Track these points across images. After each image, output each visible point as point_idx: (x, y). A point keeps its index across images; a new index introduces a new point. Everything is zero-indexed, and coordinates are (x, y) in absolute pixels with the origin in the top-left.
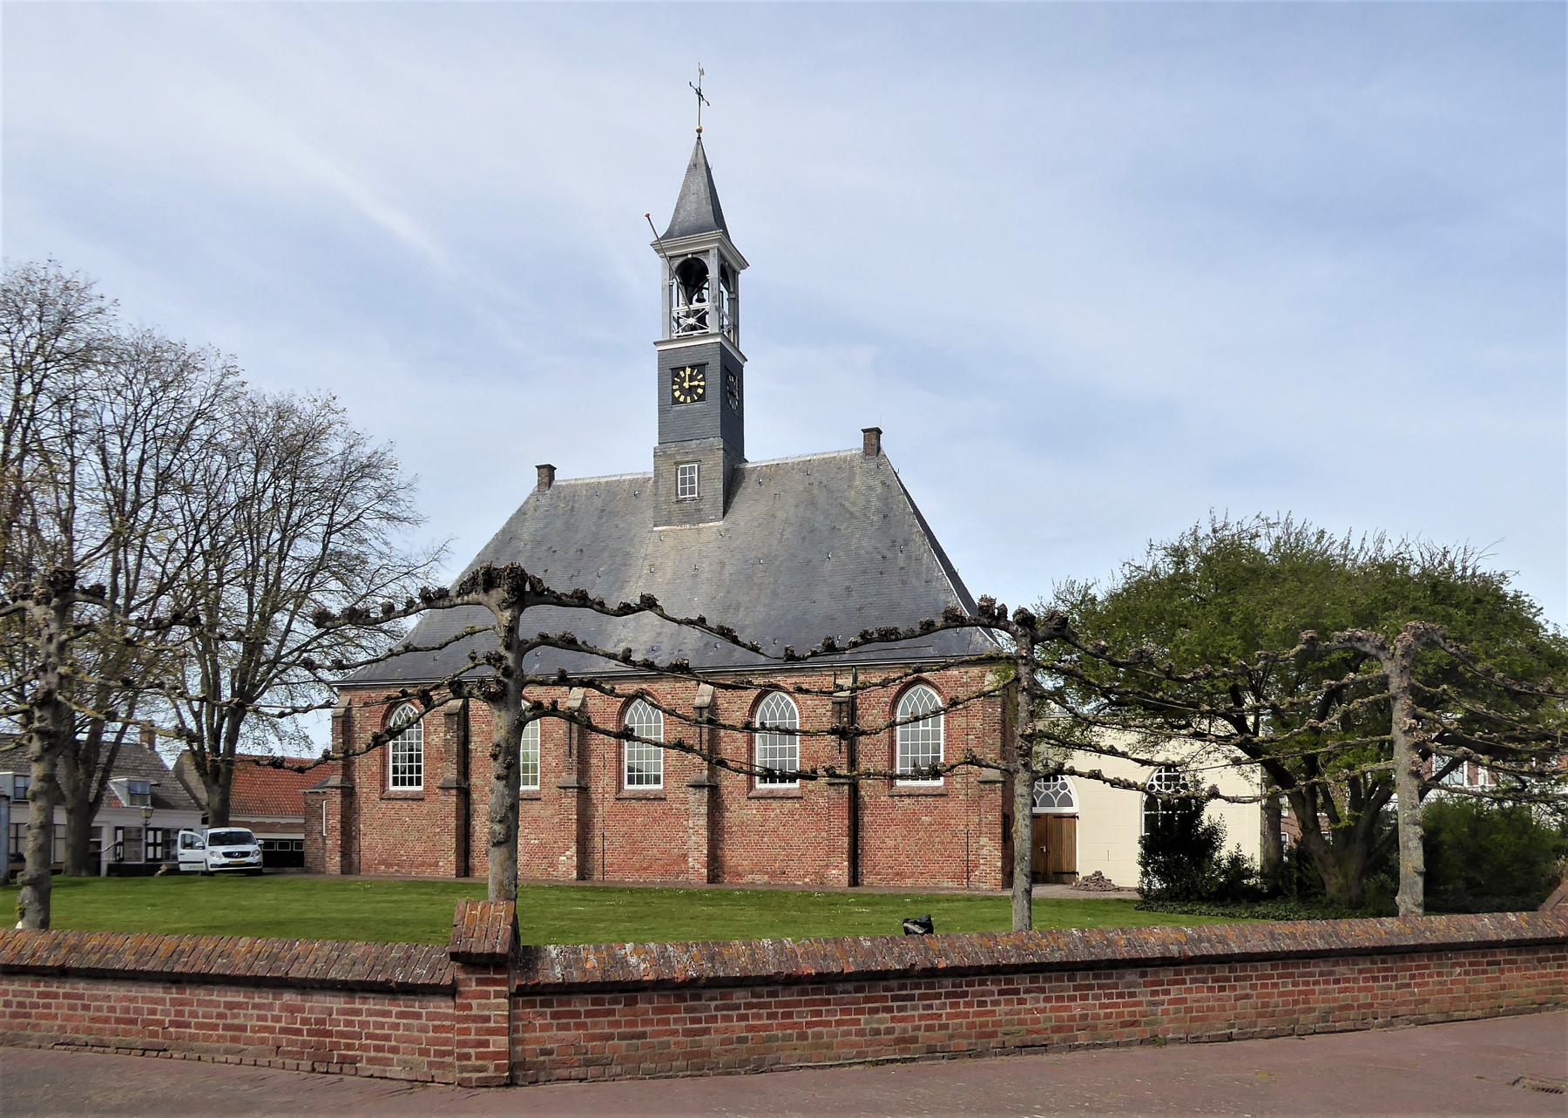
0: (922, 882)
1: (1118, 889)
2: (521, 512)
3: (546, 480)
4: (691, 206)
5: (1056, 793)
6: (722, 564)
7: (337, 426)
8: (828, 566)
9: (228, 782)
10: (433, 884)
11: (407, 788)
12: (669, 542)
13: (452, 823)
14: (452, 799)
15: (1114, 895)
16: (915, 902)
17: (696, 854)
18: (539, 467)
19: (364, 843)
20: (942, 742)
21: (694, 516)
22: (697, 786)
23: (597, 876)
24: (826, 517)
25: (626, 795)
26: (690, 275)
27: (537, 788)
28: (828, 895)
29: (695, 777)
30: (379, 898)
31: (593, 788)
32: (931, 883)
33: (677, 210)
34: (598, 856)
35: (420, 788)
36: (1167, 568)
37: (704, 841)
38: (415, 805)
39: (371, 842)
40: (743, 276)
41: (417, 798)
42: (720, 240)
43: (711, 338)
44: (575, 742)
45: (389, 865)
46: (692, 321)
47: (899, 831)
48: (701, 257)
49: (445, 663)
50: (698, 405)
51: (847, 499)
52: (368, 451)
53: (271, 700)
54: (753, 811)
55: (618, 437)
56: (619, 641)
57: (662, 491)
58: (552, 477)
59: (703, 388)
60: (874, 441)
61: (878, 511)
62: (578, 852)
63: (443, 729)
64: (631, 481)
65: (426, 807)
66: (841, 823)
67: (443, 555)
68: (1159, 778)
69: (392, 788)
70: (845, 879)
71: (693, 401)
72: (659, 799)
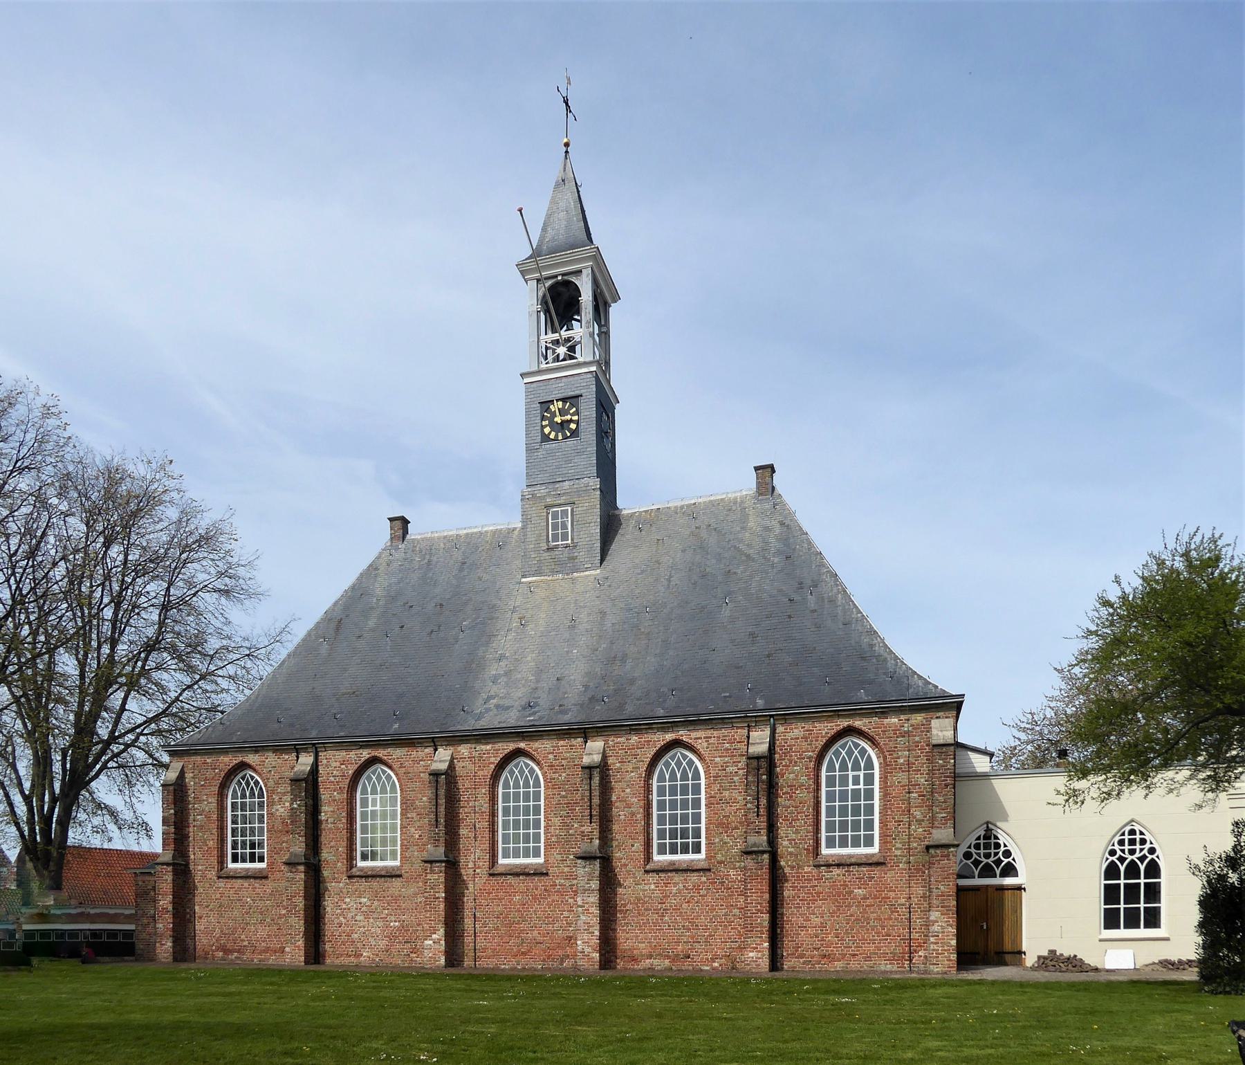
0: (854, 965)
2: (373, 568)
4: (561, 219)
5: (998, 862)
6: (603, 614)
8: (726, 612)
9: (60, 866)
10: (279, 971)
13: (300, 902)
15: (1091, 976)
18: (391, 520)
19: (200, 926)
20: (877, 802)
21: (569, 565)
22: (587, 858)
23: (468, 962)
25: (498, 870)
26: (560, 303)
27: (397, 863)
29: (584, 847)
30: (212, 989)
31: (462, 861)
32: (866, 966)
34: (468, 940)
35: (263, 865)
38: (257, 883)
40: (614, 310)
41: (260, 876)
44: (442, 809)
47: (824, 906)
48: (573, 279)
49: (292, 725)
51: (741, 541)
54: (651, 884)
55: (481, 490)
56: (490, 698)
57: (531, 537)
58: (405, 532)
59: (577, 422)
62: (447, 935)
63: (288, 797)
64: (494, 532)
65: (269, 886)
66: (759, 896)
68: (1121, 843)
69: (231, 865)
70: (765, 963)
71: (565, 438)
72: (540, 873)
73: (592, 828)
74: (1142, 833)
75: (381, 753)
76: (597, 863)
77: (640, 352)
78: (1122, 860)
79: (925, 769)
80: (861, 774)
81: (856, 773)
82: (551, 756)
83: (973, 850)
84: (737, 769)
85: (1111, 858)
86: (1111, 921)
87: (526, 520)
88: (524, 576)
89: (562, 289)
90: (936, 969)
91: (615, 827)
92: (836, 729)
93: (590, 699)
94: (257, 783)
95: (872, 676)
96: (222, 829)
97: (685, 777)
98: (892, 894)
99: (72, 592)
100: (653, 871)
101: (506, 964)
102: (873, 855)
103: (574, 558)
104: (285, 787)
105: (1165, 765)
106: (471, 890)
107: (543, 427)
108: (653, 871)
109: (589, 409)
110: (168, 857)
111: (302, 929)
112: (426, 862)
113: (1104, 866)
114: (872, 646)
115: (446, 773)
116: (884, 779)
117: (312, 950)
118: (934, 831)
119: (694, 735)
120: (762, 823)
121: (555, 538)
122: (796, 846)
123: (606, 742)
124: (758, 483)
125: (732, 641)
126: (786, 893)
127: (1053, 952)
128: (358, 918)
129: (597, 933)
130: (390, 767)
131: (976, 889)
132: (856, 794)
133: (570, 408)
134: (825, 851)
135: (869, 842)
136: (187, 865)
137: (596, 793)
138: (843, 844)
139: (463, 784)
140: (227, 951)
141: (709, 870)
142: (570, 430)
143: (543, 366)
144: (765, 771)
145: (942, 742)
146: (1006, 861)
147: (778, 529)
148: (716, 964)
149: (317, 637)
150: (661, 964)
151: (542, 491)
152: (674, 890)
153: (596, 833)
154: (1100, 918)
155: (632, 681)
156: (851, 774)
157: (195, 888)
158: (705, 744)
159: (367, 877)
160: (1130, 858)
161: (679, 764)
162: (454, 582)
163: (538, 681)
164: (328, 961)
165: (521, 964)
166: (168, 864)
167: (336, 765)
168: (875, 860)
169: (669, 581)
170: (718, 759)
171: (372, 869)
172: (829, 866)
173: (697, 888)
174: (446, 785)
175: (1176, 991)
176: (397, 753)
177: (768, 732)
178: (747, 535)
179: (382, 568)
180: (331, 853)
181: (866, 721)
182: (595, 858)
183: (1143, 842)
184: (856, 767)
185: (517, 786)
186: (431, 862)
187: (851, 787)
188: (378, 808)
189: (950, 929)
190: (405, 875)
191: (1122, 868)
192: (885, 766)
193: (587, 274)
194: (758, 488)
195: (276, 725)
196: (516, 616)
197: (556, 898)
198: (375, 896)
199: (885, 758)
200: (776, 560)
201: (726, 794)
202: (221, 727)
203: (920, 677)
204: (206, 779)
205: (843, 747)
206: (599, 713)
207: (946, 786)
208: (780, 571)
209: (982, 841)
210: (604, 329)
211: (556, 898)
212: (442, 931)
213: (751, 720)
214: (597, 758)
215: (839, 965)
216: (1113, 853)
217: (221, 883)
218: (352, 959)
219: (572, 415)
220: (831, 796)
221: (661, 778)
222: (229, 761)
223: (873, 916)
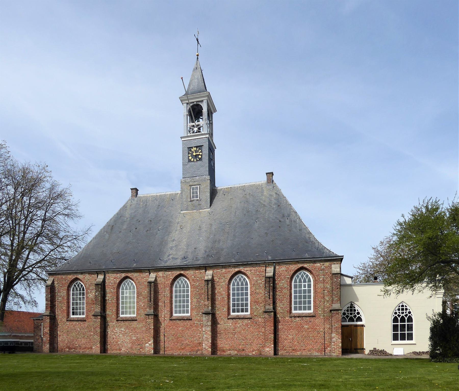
0: (304, 353)
2: (125, 207)
3: (135, 194)
5: (355, 316)
6: (211, 225)
7: (48, 178)
8: (256, 225)
13: (99, 330)
14: (99, 320)
17: (206, 342)
18: (131, 189)
19: (59, 339)
21: (198, 207)
23: (162, 352)
26: (195, 112)
27: (135, 315)
29: (205, 310)
32: (308, 353)
34: (162, 344)
36: (412, 218)
37: (210, 337)
38: (82, 323)
39: (63, 339)
40: (214, 115)
41: (83, 320)
43: (202, 139)
44: (152, 295)
45: (70, 349)
47: (294, 332)
48: (200, 104)
50: (199, 162)
52: (60, 189)
53: (19, 288)
57: (184, 196)
58: (137, 194)
59: (201, 155)
61: (275, 204)
63: (94, 291)
64: (170, 195)
65: (86, 324)
67: (89, 232)
68: (399, 310)
70: (272, 352)
72: (189, 319)
73: (208, 303)
74: (406, 306)
75: (129, 275)
80: (307, 284)
81: (305, 284)
82: (193, 276)
83: (346, 312)
84: (262, 281)
85: (395, 315)
86: (395, 338)
87: (182, 190)
88: (181, 211)
90: (334, 354)
91: (217, 303)
94: (82, 285)
95: (310, 249)
96: (68, 302)
98: (318, 327)
100: (231, 319)
101: (176, 353)
102: (311, 313)
103: (200, 205)
107: (189, 157)
108: (231, 319)
109: (206, 150)
111: (99, 340)
114: (310, 238)
116: (315, 286)
117: (103, 348)
119: (246, 269)
120: (271, 301)
121: (193, 197)
122: (283, 310)
123: (213, 271)
124: (267, 179)
126: (279, 327)
127: (375, 349)
128: (120, 336)
130: (133, 280)
132: (305, 291)
134: (293, 312)
135: (309, 308)
136: (55, 316)
137: (210, 290)
138: (300, 309)
139: (160, 287)
140: (70, 349)
141: (251, 318)
142: (199, 158)
143: (189, 135)
144: (272, 282)
145: (336, 273)
146: (358, 316)
148: (254, 353)
149: (105, 232)
150: (233, 353)
151: (188, 180)
152: (239, 325)
153: (210, 304)
154: (391, 337)
155: (222, 250)
156: (303, 284)
157: (58, 325)
158: (250, 273)
159: (124, 320)
160: (402, 315)
162: (155, 212)
163: (187, 249)
164: (109, 352)
166: (48, 316)
167: (112, 279)
168: (312, 315)
169: (235, 213)
170: (254, 278)
171: (126, 317)
172: (295, 317)
173: (247, 325)
174: (154, 287)
176: (135, 275)
177: (273, 268)
179: (128, 207)
180: (110, 312)
181: (308, 265)
182: (209, 314)
183: (406, 309)
184: (305, 281)
185: (180, 287)
186: (148, 315)
187: (303, 288)
188: (128, 295)
190: (138, 320)
191: (399, 319)
192: (315, 281)
193: (205, 102)
194: (267, 181)
199: (315, 278)
200: (274, 206)
201: (258, 290)
205: (300, 274)
206: (211, 261)
207: (337, 288)
208: (276, 211)
209: (349, 309)
212: (152, 341)
213: (266, 264)
214: (210, 277)
215: (299, 353)
216: (396, 313)
217: (68, 323)
219: (200, 152)
220: (296, 292)
221: (234, 285)
222: (71, 277)
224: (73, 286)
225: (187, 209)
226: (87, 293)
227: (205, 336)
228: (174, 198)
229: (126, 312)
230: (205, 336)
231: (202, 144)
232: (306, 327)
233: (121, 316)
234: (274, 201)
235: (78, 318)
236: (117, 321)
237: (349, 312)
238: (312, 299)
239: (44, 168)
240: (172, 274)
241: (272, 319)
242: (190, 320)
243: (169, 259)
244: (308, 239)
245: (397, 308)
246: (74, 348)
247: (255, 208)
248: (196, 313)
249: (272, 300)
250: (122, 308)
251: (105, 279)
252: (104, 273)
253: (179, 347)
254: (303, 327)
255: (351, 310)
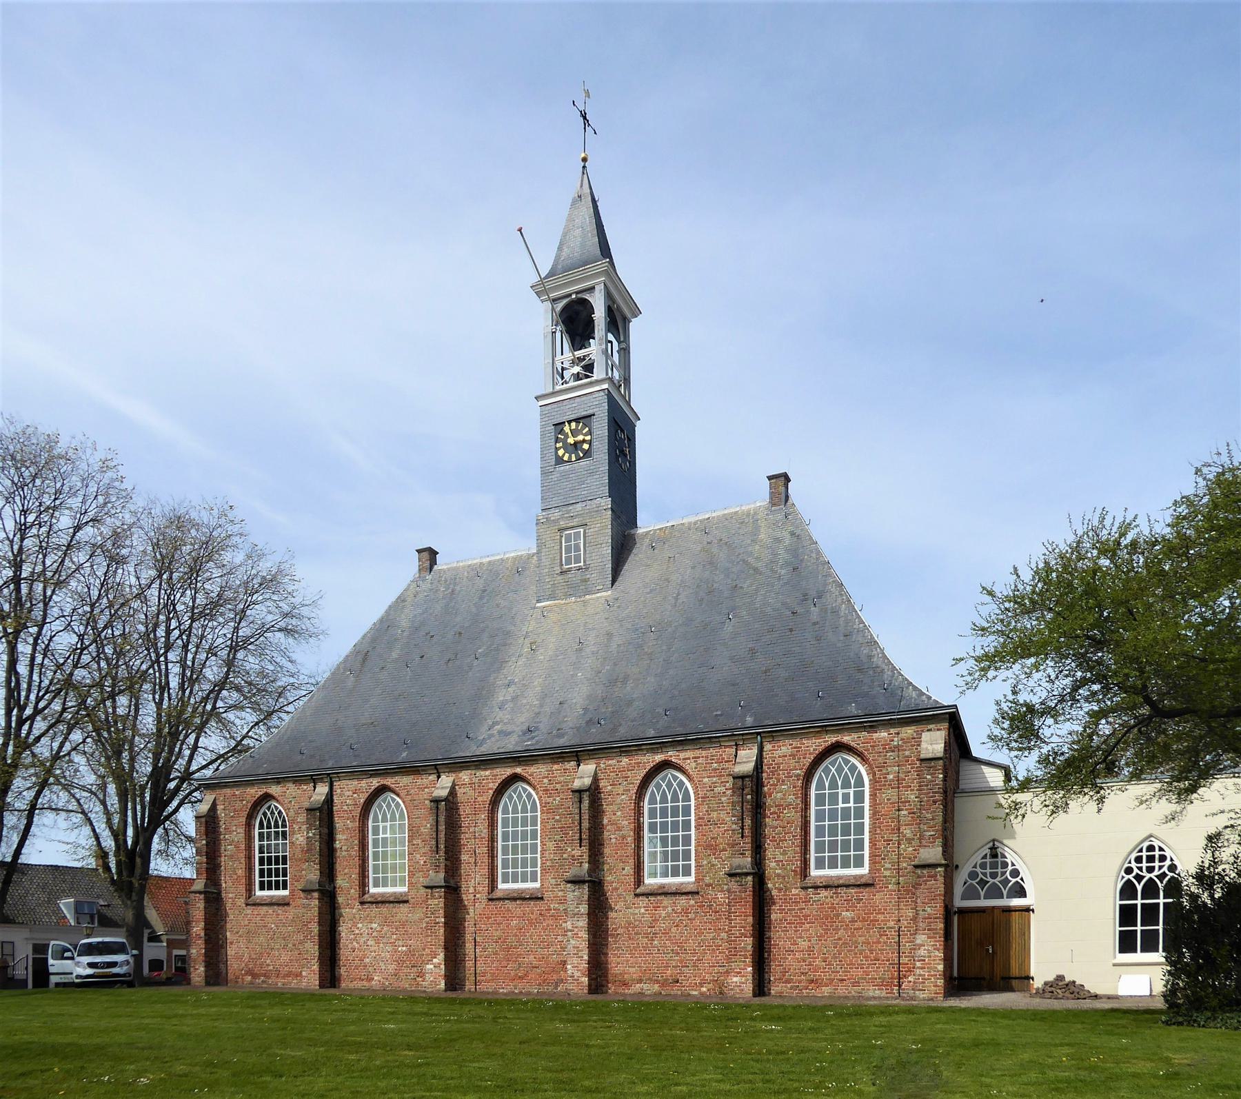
0: (842, 990)
1: (1096, 996)
2: (401, 600)
3: (427, 564)
5: (1007, 881)
7: (235, 539)
8: (729, 628)
11: (273, 893)
12: (553, 617)
13: (315, 928)
15: (1087, 1004)
16: (839, 1015)
18: (419, 551)
19: (231, 951)
20: (867, 821)
21: (581, 588)
22: (576, 882)
23: (469, 986)
24: (727, 576)
26: (575, 322)
27: (405, 889)
28: (727, 1007)
32: (854, 991)
33: (560, 248)
34: (469, 964)
35: (286, 893)
38: (280, 910)
39: (237, 951)
40: (635, 326)
42: (606, 273)
44: (442, 836)
45: (254, 976)
46: (577, 369)
47: (813, 930)
48: (587, 296)
49: (312, 756)
50: (583, 463)
58: (433, 562)
59: (590, 443)
60: (782, 489)
61: (787, 564)
62: (447, 959)
64: (515, 559)
65: (291, 912)
66: (744, 920)
68: (1139, 860)
69: (259, 893)
71: (579, 459)
72: (536, 898)
73: (582, 852)
74: (1161, 849)
75: (389, 781)
76: (586, 886)
77: (662, 368)
78: (1139, 878)
79: (915, 785)
80: (851, 791)
81: (846, 791)
82: (546, 781)
83: (978, 870)
84: (725, 789)
85: (1127, 877)
86: (1127, 943)
87: (541, 545)
88: (538, 601)
89: (577, 307)
90: (921, 995)
91: (607, 851)
92: (824, 745)
93: (587, 723)
94: (280, 813)
95: (866, 688)
96: (249, 858)
97: (675, 798)
98: (881, 917)
99: (149, 639)
100: (643, 895)
101: (505, 988)
102: (862, 876)
103: (586, 581)
104: (302, 818)
105: (1137, 776)
106: (472, 914)
107: (557, 449)
108: (643, 895)
109: (601, 428)
110: (199, 885)
111: (317, 954)
112: (427, 887)
113: (1120, 886)
114: (870, 657)
115: (446, 799)
116: (873, 796)
117: (328, 975)
118: (922, 850)
119: (682, 755)
120: (747, 844)
121: (568, 561)
122: (783, 868)
123: (598, 765)
124: (771, 493)
125: (731, 658)
126: (773, 917)
127: (1060, 978)
128: (369, 943)
129: (586, 957)
130: (398, 795)
131: (982, 910)
132: (846, 812)
133: (583, 429)
134: (814, 872)
135: (859, 862)
136: (219, 893)
137: (586, 817)
138: (833, 865)
139: (464, 810)
140: (254, 976)
141: (697, 893)
142: (583, 450)
143: (558, 388)
144: (752, 790)
145: (930, 756)
146: (1014, 880)
147: (787, 541)
148: (704, 989)
149: (345, 670)
150: (650, 988)
151: (555, 514)
152: (663, 913)
153: (586, 857)
154: (1113, 940)
155: (630, 703)
156: (841, 792)
157: (226, 915)
158: (694, 765)
159: (377, 903)
160: (1148, 876)
161: (669, 785)
162: (474, 610)
163: (541, 706)
164: (343, 985)
165: (519, 987)
166: (200, 893)
167: (349, 793)
168: (863, 881)
169: (676, 599)
171: (383, 895)
172: (816, 887)
173: (686, 911)
174: (448, 812)
175: (1135, 1020)
176: (404, 781)
177: (755, 751)
178: (757, 547)
179: (409, 599)
180: (345, 880)
181: (855, 736)
182: (584, 882)
183: (1163, 858)
184: (846, 785)
185: (515, 811)
186: (431, 888)
187: (841, 805)
188: (388, 835)
189: (937, 953)
190: (412, 901)
191: (1139, 888)
192: (874, 782)
193: (600, 290)
194: (771, 498)
195: (300, 757)
196: (527, 641)
197: (551, 922)
198: (385, 922)
199: (874, 774)
200: (783, 572)
201: (714, 815)
202: (251, 760)
203: (915, 688)
204: (235, 811)
205: (833, 764)
206: (596, 735)
207: (935, 802)
208: (786, 584)
209: (988, 860)
210: (623, 345)
211: (551, 922)
212: (442, 956)
213: (738, 738)
214: (587, 781)
215: (826, 991)
216: (1129, 871)
217: (249, 910)
218: (365, 983)
219: (586, 435)
220: (820, 817)
221: (653, 800)
222: (255, 792)
223: (861, 939)
224: (260, 815)
225: (552, 597)
226: (293, 833)
227: (573, 942)
228: (524, 569)
229: (385, 879)
230: (573, 942)
231: (590, 412)
232: (847, 915)
233: (373, 890)
234: (783, 555)
235: (272, 897)
236: (362, 903)
237: (988, 871)
238: (866, 837)
239: (223, 514)
240: (492, 777)
241: (748, 895)
242: (537, 898)
243: (492, 735)
244: (865, 660)
245: (1134, 855)
246: (265, 975)
247: (729, 581)
248: (553, 882)
249: (748, 840)
250: (376, 871)
251: (762, 762)
252: (330, 778)
253: (513, 973)
254: (838, 915)
255: (994, 866)
